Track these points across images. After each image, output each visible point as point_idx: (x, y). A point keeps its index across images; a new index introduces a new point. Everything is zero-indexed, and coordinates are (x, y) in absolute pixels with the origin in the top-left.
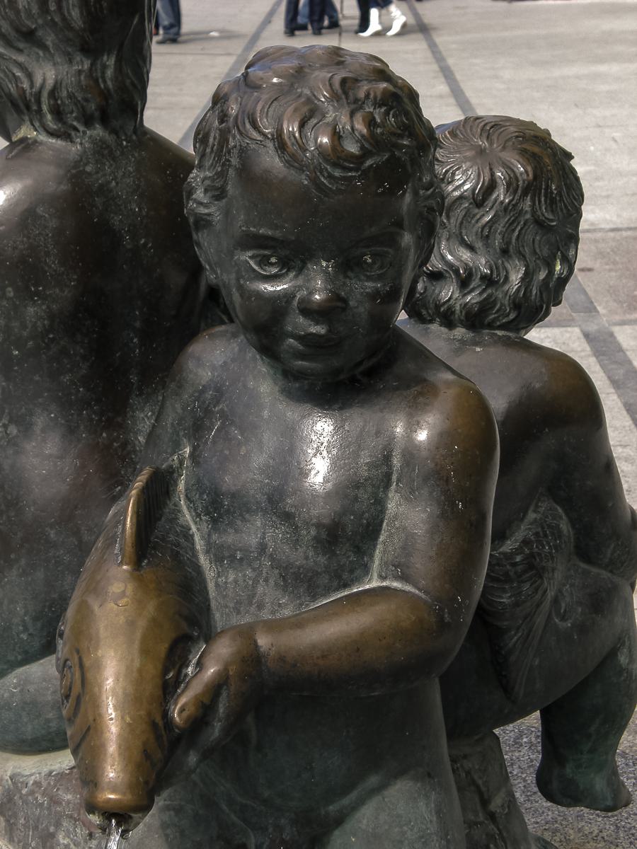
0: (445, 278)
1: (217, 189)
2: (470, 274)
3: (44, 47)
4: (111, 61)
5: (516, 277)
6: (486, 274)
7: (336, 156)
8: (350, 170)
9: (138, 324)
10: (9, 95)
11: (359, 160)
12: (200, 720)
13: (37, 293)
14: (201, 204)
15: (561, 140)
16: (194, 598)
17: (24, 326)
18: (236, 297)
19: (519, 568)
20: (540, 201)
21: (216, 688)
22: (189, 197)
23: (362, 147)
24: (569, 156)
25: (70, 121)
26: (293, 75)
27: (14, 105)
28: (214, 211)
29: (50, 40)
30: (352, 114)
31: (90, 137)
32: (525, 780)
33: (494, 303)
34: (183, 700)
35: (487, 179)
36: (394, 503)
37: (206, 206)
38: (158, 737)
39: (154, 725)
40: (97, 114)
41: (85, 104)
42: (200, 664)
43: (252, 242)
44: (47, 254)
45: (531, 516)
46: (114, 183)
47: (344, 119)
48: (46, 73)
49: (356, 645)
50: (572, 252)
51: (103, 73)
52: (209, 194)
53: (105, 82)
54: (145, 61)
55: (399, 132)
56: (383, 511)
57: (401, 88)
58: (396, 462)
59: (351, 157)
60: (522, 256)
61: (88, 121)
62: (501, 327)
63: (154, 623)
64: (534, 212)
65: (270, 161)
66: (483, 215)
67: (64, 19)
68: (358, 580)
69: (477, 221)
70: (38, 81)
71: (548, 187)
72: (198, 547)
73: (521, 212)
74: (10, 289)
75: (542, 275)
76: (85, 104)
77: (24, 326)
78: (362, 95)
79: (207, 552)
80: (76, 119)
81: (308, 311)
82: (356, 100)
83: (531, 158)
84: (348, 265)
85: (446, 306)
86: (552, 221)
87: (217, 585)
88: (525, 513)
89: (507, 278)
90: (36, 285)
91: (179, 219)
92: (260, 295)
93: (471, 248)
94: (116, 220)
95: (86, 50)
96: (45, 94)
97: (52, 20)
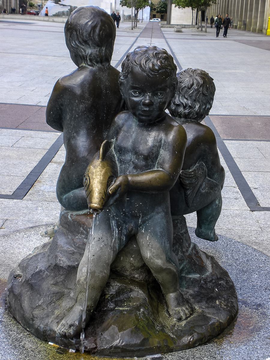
0: (180, 106)
1: (126, 76)
2: (186, 105)
3: (89, 45)
4: (104, 49)
5: (197, 107)
6: (190, 105)
7: (152, 70)
8: (156, 72)
9: (105, 112)
10: (80, 55)
11: (158, 70)
12: (114, 193)
13: (83, 102)
14: (122, 79)
15: (211, 75)
16: (111, 210)
17: (79, 110)
18: (128, 101)
19: (194, 178)
20: (204, 89)
21: (119, 186)
22: (119, 78)
23: (159, 68)
24: (213, 80)
25: (93, 62)
26: (145, 51)
27: (81, 58)
28: (124, 81)
29: (90, 43)
30: (157, 60)
31: (98, 66)
32: (195, 240)
33: (192, 112)
34: (112, 188)
35: (192, 83)
36: (162, 152)
37: (123, 80)
38: (105, 195)
39: (105, 192)
40: (100, 61)
41: (97, 58)
42: (115, 182)
43: (133, 88)
44: (86, 93)
45: (197, 165)
46: (102, 77)
47: (155, 61)
48: (89, 51)
49: (150, 181)
50: (211, 102)
51: (102, 51)
52: (124, 77)
53: (102, 53)
54: (112, 50)
55: (167, 65)
56: (159, 153)
57: (169, 56)
58: (163, 142)
59: (156, 70)
60: (199, 102)
61: (97, 62)
62: (193, 119)
63: (106, 173)
64: (202, 92)
65: (137, 69)
66: (190, 91)
67: (94, 38)
68: (152, 168)
69: (189, 92)
70: (87, 52)
71: (206, 86)
72: (116, 159)
73: (199, 91)
74: (77, 100)
75: (204, 107)
76: (97, 58)
77: (79, 110)
78: (160, 56)
79: (118, 161)
80: (95, 62)
81: (145, 105)
82: (158, 58)
83: (203, 78)
84: (154, 94)
85: (180, 113)
86: (207, 94)
87: (120, 168)
88: (196, 164)
89: (195, 107)
90: (83, 100)
91: (108, 210)
92: (133, 101)
93: (187, 99)
94: (102, 86)
95: (98, 46)
96: (88, 56)
97: (91, 38)
